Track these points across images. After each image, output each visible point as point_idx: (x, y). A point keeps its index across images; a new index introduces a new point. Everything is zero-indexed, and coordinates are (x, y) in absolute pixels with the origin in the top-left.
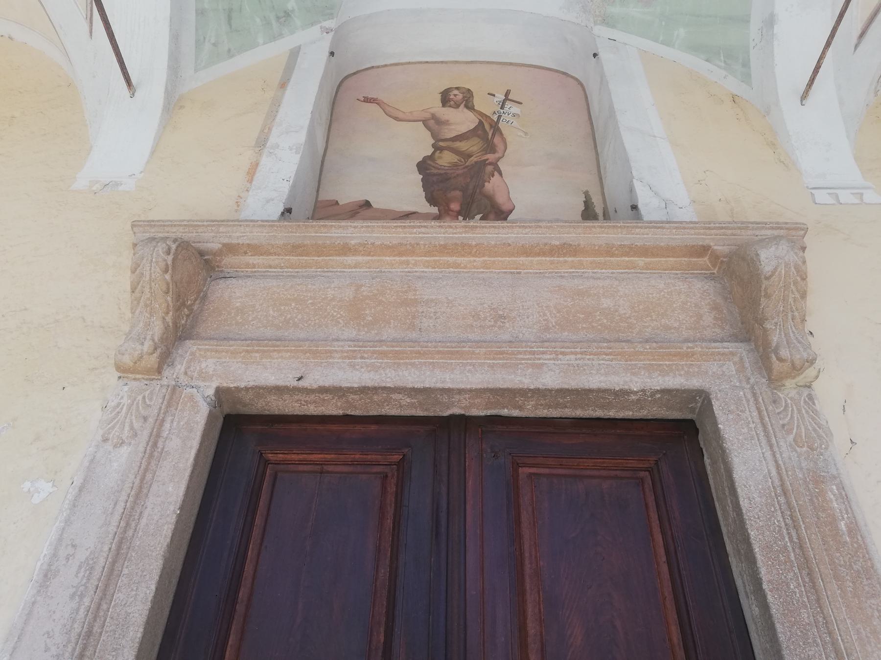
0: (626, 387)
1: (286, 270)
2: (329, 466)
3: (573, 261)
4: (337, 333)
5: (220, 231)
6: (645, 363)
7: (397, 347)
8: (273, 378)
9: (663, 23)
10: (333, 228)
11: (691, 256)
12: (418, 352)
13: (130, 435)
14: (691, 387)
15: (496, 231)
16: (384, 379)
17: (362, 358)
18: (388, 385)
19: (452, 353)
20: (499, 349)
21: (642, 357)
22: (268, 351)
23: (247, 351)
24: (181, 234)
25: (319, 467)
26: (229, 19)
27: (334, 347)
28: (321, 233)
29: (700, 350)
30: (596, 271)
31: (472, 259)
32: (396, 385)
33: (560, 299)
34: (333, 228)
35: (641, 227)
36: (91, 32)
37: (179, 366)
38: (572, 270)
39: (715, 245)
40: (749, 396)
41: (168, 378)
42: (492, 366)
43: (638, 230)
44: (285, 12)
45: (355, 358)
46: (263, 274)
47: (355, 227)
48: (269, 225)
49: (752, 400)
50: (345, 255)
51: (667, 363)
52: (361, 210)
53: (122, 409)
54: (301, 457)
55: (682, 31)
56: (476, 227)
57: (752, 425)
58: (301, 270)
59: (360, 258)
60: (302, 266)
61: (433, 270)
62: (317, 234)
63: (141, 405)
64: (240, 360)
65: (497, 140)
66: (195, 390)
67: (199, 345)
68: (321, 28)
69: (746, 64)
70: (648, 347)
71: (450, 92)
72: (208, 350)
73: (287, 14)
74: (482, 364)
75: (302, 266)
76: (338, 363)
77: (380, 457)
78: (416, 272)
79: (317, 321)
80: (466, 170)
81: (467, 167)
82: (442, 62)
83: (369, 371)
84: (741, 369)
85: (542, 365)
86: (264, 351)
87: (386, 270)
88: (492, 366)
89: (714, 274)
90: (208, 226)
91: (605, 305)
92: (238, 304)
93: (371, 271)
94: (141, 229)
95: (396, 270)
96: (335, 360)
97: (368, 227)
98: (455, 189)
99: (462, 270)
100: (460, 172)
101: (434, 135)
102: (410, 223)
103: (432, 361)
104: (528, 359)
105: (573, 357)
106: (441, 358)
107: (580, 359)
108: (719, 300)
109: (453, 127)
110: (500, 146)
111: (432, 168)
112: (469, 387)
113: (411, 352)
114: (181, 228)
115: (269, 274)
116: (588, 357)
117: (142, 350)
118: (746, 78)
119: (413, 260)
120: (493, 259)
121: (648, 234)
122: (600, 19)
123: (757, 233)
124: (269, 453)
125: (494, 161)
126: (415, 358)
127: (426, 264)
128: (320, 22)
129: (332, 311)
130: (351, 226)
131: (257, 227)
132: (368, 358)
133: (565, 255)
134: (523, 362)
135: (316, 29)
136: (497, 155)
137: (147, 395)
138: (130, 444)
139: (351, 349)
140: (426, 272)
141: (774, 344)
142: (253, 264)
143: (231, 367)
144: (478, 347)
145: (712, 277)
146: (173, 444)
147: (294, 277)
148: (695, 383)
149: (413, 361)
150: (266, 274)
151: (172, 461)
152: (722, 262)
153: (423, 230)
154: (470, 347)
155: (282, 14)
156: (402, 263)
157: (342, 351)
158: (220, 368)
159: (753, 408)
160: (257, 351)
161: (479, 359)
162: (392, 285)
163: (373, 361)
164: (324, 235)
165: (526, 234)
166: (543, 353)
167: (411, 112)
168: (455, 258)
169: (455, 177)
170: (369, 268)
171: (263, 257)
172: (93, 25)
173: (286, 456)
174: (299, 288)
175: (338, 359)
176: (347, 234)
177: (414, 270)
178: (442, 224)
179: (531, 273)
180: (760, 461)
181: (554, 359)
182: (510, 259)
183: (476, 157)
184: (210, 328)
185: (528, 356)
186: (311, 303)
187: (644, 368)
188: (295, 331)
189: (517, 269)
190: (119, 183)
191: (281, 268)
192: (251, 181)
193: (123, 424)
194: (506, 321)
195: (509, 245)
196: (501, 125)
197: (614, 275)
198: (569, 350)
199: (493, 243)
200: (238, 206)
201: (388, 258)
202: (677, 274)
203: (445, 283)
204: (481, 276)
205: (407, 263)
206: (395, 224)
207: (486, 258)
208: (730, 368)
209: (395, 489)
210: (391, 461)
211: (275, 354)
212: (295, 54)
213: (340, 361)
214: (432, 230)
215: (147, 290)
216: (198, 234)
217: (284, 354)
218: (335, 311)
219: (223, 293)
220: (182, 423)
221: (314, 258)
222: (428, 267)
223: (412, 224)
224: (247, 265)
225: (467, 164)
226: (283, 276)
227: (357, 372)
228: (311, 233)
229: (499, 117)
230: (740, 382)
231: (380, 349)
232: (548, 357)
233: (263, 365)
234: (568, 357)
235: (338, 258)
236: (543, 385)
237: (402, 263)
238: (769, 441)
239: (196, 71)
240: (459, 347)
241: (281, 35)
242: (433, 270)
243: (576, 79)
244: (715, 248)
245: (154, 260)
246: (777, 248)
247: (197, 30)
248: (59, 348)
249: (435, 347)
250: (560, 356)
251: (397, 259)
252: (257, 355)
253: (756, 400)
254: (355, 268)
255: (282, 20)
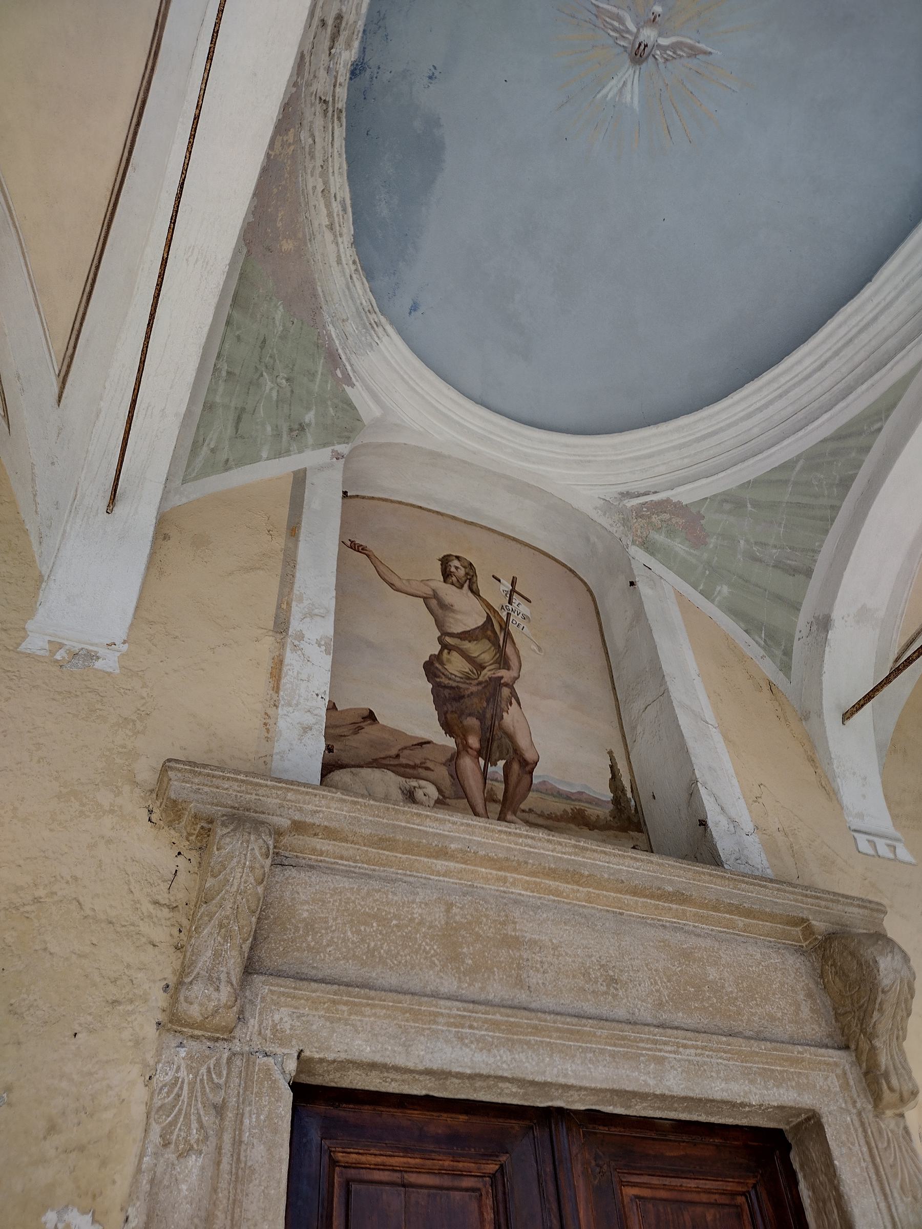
0: (747, 1100)
1: (360, 865)
2: (411, 1174)
3: (677, 910)
4: (435, 981)
5: (288, 798)
6: (759, 1066)
7: (512, 1017)
8: (368, 1049)
9: (707, 572)
10: (428, 820)
11: (787, 924)
12: (535, 1027)
13: (201, 1138)
14: (804, 1106)
15: (607, 858)
16: (499, 1064)
17: (471, 1027)
18: (505, 1074)
19: (571, 1032)
20: (621, 1033)
21: (757, 1059)
22: (361, 1004)
23: (334, 1002)
24: (235, 793)
25: (398, 1175)
26: (239, 420)
27: (440, 1008)
28: (414, 824)
29: (809, 1056)
30: (697, 924)
31: (576, 887)
32: (514, 1075)
33: (668, 961)
34: (428, 820)
35: (747, 883)
36: (60, 397)
37: (252, 1021)
38: (674, 920)
39: (813, 920)
40: (857, 1124)
41: (242, 1040)
42: (613, 1055)
43: (743, 886)
44: (300, 424)
45: (463, 1027)
46: (330, 866)
47: (454, 823)
48: (352, 801)
49: (860, 1130)
50: (437, 858)
51: (779, 1068)
52: (366, 723)
53: (181, 1088)
54: (379, 1160)
55: (725, 589)
56: (587, 849)
57: (863, 1165)
58: (378, 868)
59: (452, 865)
60: (381, 863)
61: (531, 894)
62: (408, 825)
63: (207, 1083)
64: (322, 1013)
65: (509, 650)
66: (271, 1060)
67: (272, 985)
68: (333, 451)
69: (788, 653)
70: (763, 1047)
71: (450, 561)
72: (283, 994)
73: (302, 428)
74: (602, 1052)
75: (381, 863)
76: (442, 1031)
77: (473, 1165)
78: (512, 893)
79: (408, 957)
80: (480, 688)
81: (480, 683)
82: (438, 513)
83: (481, 1050)
84: (845, 1086)
85: (664, 1058)
86: (355, 1004)
87: (479, 885)
88: (613, 1055)
89: (802, 947)
90: (274, 787)
91: (711, 977)
92: (305, 915)
93: (462, 884)
94: (179, 775)
95: (491, 887)
96: (439, 1027)
97: (468, 825)
98: (470, 715)
99: (563, 900)
100: (474, 689)
101: (439, 624)
102: (516, 829)
103: (548, 1040)
104: (649, 1049)
105: (693, 1051)
106: (560, 1038)
107: (700, 1055)
108: (812, 986)
109: (459, 617)
110: (514, 662)
111: (443, 677)
112: (593, 1085)
113: (528, 1026)
114: (237, 784)
115: (338, 866)
116: (707, 1053)
117: (219, 1000)
118: (786, 668)
119: (512, 877)
120: (597, 892)
121: (752, 893)
122: (640, 540)
123: (846, 909)
124: (339, 1152)
125: (509, 682)
126: (531, 1034)
127: (526, 885)
128: (333, 445)
129: (424, 943)
130: (449, 821)
131: (336, 801)
132: (477, 1029)
133: (671, 902)
134: (644, 1052)
135: (328, 451)
136: (513, 673)
137: (212, 1067)
138: (201, 1153)
139: (459, 1013)
140: (523, 895)
141: (883, 1068)
142: (321, 850)
143: (312, 1025)
144: (600, 1028)
145: (800, 951)
146: (257, 1154)
147: (370, 877)
148: (807, 1100)
149: (528, 1038)
150: (334, 866)
151: (260, 1185)
152: (816, 939)
153: (529, 841)
154: (591, 1027)
155: (296, 427)
156: (498, 879)
157: (449, 1016)
158: (299, 1024)
159: (862, 1142)
160: (346, 1003)
161: (599, 1043)
162: (486, 909)
163: (483, 1033)
164: (416, 827)
165: (637, 869)
166: (665, 1043)
167: (408, 580)
168: (557, 883)
169: (468, 696)
170: (460, 879)
171: (336, 843)
172: (66, 387)
173: (360, 1157)
174: (377, 896)
175: (443, 1026)
176: (444, 830)
177: (511, 890)
178: (551, 837)
179: (633, 916)
180: (876, 1213)
181: (675, 1052)
182: (615, 895)
183: (490, 670)
184: (275, 952)
185: (649, 1046)
186: (396, 926)
187: (760, 1074)
188: (384, 971)
189: (620, 908)
190: (93, 654)
191: (355, 861)
192: (277, 689)
193: (188, 1115)
194: (618, 987)
195: (622, 882)
196: (512, 628)
197: (714, 933)
198: (690, 1043)
199: (606, 876)
200: (268, 731)
201: (484, 870)
202: (771, 942)
203: (545, 915)
204: (581, 910)
205: (505, 880)
206: (499, 828)
207: (590, 890)
208: (834, 1083)
209: (492, 1216)
210: (484, 1171)
211: (368, 1011)
212: (300, 479)
213: (445, 1028)
214: (539, 845)
215: (228, 905)
216: (257, 797)
217: (378, 1011)
218: (427, 944)
219: (283, 892)
220: (262, 1117)
221: (396, 854)
222: (526, 890)
223: (518, 831)
224: (314, 851)
225: (481, 679)
226: (355, 873)
227: (467, 1050)
228: (401, 821)
229: (509, 615)
230: (846, 1103)
231: (493, 1017)
232: (669, 1048)
233: (353, 1025)
234: (688, 1051)
235: (426, 860)
236: (669, 1091)
237: (498, 879)
238: (883, 1189)
239: (184, 481)
240: (580, 1025)
241: (288, 452)
242: (531, 894)
243: (585, 584)
244: (814, 922)
245: (248, 863)
246: (893, 958)
247: (198, 427)
248: (51, 954)
249: (555, 1022)
250: (681, 1049)
251: (494, 872)
252: (345, 1008)
253: (865, 1131)
254: (444, 876)
255: (295, 433)
